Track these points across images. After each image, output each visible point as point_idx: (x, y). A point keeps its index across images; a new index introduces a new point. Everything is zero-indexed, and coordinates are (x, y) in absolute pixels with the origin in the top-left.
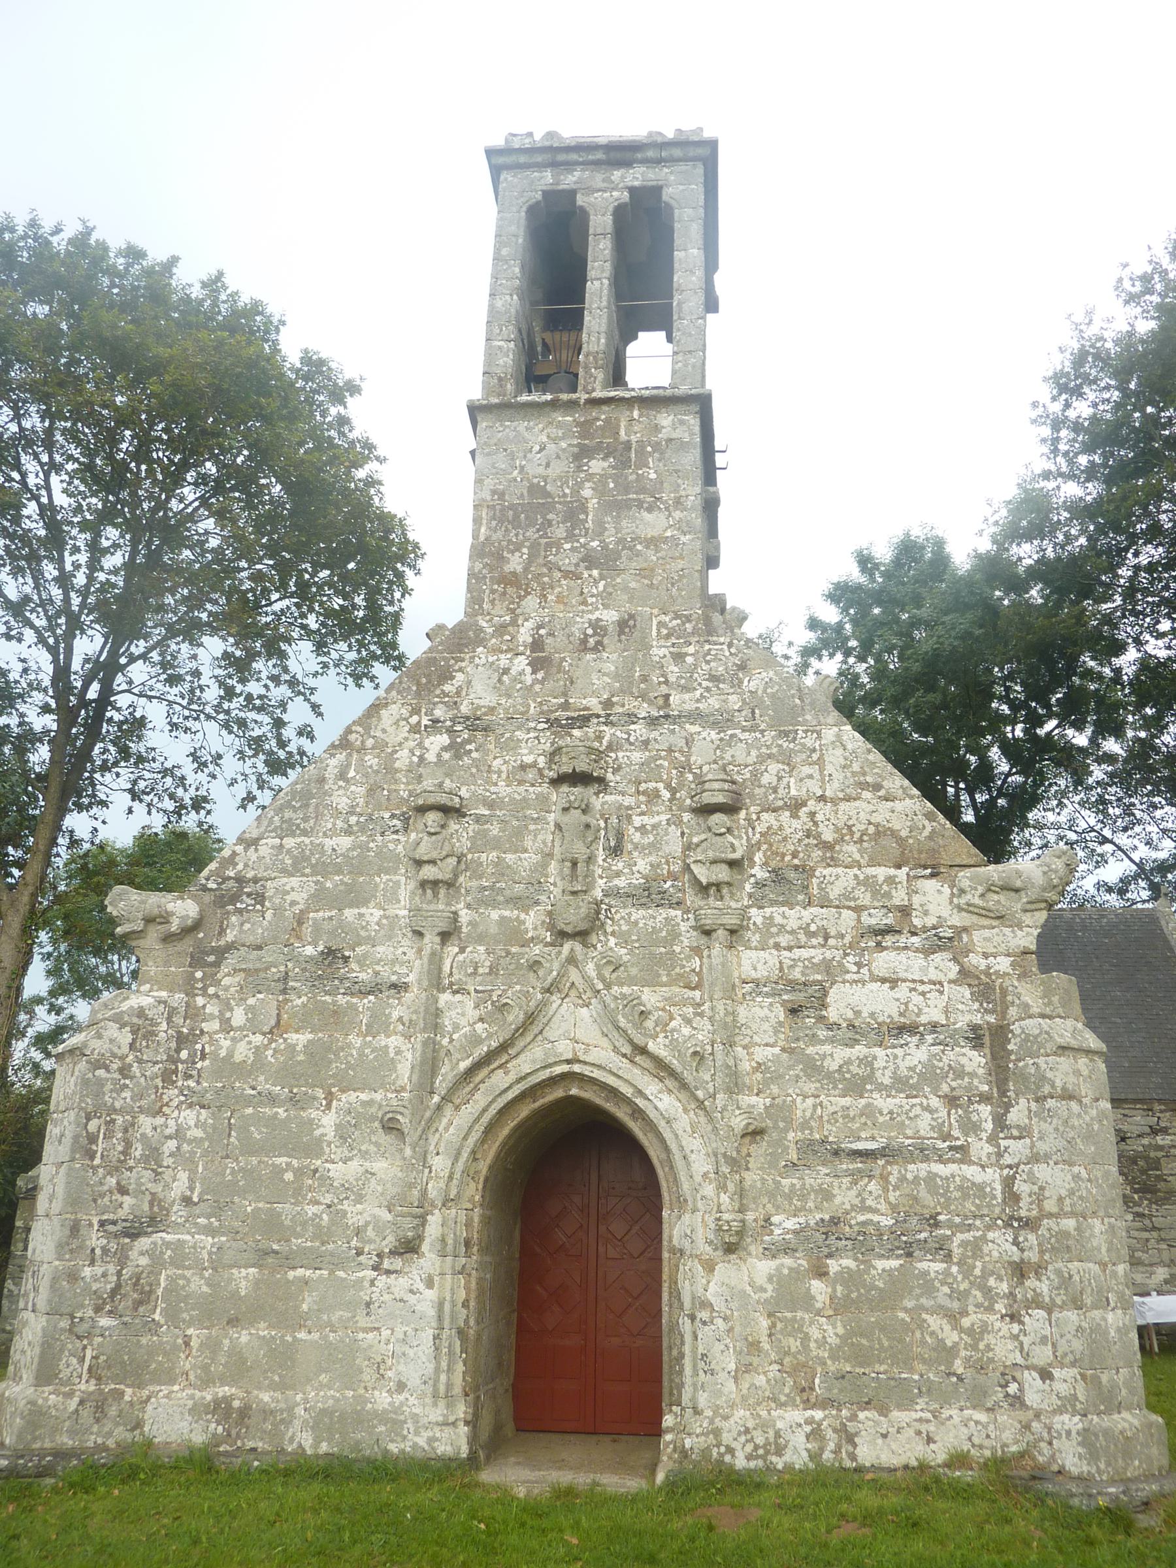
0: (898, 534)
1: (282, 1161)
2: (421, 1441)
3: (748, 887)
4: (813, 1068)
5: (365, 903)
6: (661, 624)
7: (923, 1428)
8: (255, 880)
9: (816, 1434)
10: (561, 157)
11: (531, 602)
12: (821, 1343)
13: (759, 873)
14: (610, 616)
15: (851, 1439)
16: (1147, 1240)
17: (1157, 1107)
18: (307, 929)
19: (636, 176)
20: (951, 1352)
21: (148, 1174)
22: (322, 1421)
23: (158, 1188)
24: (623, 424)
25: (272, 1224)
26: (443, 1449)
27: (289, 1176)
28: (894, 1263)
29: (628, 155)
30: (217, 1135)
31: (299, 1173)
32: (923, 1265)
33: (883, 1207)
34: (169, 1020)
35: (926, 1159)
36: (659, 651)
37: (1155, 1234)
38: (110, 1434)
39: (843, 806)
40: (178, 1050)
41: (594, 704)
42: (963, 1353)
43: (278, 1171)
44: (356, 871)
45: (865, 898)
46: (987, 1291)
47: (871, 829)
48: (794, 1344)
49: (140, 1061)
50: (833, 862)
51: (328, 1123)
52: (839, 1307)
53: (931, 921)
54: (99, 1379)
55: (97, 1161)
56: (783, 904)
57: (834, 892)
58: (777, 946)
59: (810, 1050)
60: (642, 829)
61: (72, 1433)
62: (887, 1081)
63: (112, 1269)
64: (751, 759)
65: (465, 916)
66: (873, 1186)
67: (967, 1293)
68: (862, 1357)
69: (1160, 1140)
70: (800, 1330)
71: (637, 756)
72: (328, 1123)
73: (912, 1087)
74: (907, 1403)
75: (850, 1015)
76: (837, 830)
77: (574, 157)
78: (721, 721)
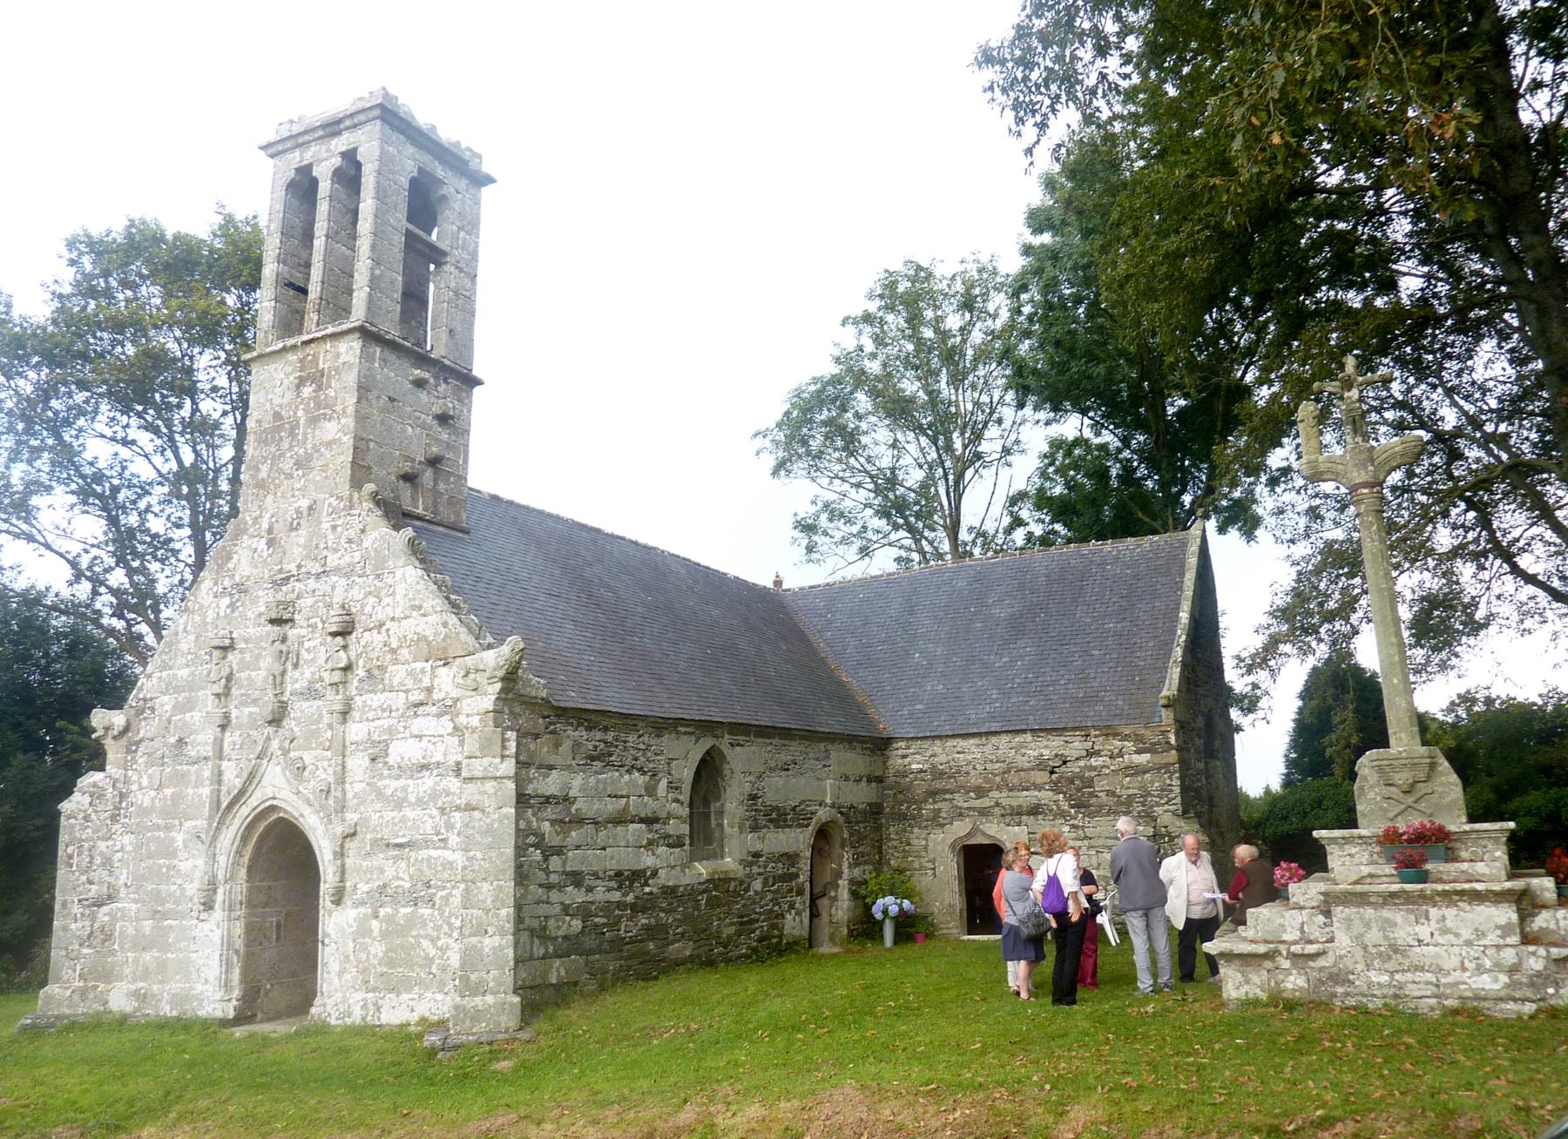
1: (161, 861)
2: (210, 1010)
3: (355, 683)
4: (380, 794)
5: (191, 710)
6: (330, 505)
7: (411, 1003)
8: (151, 699)
9: (364, 1007)
10: (301, 140)
11: (270, 498)
12: (376, 955)
14: (304, 503)
15: (378, 1009)
17: (1093, 733)
18: (172, 727)
19: (341, 144)
20: (431, 961)
21: (106, 872)
22: (177, 1000)
23: (112, 880)
24: (322, 355)
25: (158, 897)
27: (164, 870)
28: (409, 910)
29: (329, 130)
30: (138, 847)
31: (168, 868)
32: (422, 911)
33: (406, 877)
34: (114, 786)
35: (427, 848)
36: (326, 526)
37: (1086, 842)
38: (90, 1007)
39: (404, 622)
40: (120, 802)
41: (292, 567)
42: (437, 961)
43: (161, 867)
44: (191, 690)
45: (410, 684)
46: (450, 925)
47: (416, 637)
48: (363, 956)
49: (96, 812)
50: (395, 662)
51: (180, 838)
52: (385, 935)
53: (442, 695)
54: (85, 980)
55: (74, 868)
56: (371, 692)
57: (396, 682)
58: (367, 720)
59: (379, 783)
60: (308, 650)
61: (69, 1007)
62: (413, 800)
63: (87, 923)
64: (362, 596)
66: (403, 865)
67: (441, 926)
68: (391, 964)
69: (1094, 762)
70: (366, 949)
72: (180, 838)
73: (425, 803)
74: (409, 990)
75: (399, 760)
76: (399, 640)
77: (307, 138)
78: (348, 572)
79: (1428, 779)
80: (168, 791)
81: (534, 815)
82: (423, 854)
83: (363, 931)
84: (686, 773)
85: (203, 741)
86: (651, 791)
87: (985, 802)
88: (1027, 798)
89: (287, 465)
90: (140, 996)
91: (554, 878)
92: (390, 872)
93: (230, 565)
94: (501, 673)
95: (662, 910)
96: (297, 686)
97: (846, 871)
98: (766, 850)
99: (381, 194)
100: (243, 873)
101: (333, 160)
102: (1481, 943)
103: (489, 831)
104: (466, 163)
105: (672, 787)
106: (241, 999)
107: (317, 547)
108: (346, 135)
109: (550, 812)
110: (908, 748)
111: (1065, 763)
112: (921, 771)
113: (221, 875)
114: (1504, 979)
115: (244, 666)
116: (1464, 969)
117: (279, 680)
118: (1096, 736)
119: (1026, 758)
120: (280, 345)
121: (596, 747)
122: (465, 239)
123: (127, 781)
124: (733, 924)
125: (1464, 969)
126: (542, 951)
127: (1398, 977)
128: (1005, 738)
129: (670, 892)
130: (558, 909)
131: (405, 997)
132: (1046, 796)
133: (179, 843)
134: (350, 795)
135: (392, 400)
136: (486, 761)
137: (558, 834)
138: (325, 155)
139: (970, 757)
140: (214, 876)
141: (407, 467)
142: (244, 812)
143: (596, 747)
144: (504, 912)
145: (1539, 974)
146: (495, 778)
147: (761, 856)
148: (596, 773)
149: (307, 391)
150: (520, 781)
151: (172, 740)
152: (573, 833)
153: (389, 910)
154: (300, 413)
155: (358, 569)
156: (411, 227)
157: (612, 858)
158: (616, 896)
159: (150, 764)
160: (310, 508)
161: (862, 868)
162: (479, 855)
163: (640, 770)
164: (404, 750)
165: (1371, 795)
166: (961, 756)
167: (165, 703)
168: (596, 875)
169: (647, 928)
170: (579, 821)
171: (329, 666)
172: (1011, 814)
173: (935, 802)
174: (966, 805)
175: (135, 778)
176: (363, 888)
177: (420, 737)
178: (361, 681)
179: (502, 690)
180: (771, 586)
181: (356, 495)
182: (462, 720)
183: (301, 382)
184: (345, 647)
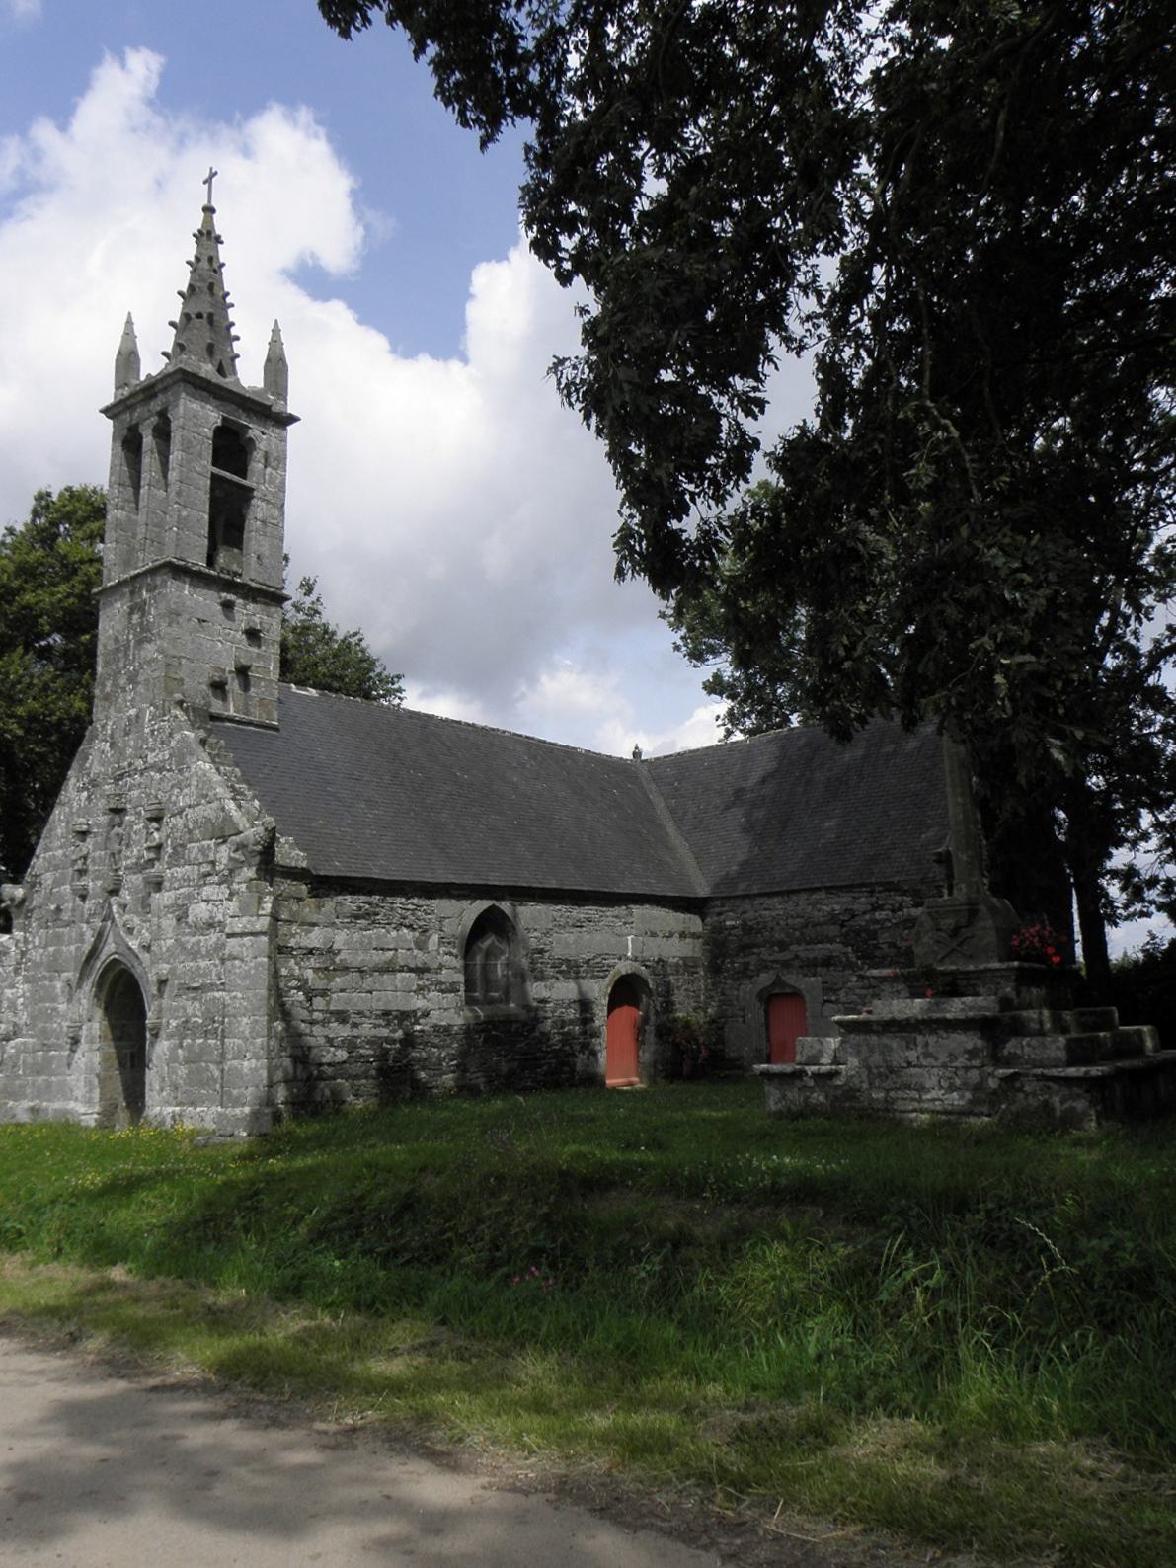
13: (169, 850)
16: (866, 996)
17: (878, 888)
28: (201, 1040)
33: (200, 1014)
34: (16, 946)
37: (870, 991)
39: (196, 809)
77: (133, 401)
79: (969, 924)
81: (296, 964)
83: (172, 1059)
86: (421, 945)
87: (787, 955)
88: (820, 950)
89: (122, 682)
91: (317, 1015)
93: (87, 765)
97: (653, 1018)
98: (554, 997)
102: (954, 1065)
103: (246, 976)
104: (269, 407)
107: (142, 748)
109: (313, 961)
110: (722, 906)
111: (853, 917)
112: (733, 927)
114: (968, 1095)
118: (880, 892)
119: (821, 914)
121: (360, 908)
124: (515, 1060)
127: (892, 1094)
128: (804, 896)
132: (836, 948)
136: (245, 920)
137: (322, 979)
138: (147, 414)
139: (774, 914)
142: (98, 965)
143: (360, 908)
144: (259, 1040)
145: (995, 1092)
146: (252, 934)
147: (548, 1003)
148: (361, 929)
149: (136, 618)
150: (272, 932)
151: (53, 907)
153: (189, 1041)
154: (131, 637)
156: (216, 470)
157: (379, 1000)
158: (385, 1032)
159: (40, 927)
160: (137, 716)
162: (239, 995)
163: (410, 927)
164: (200, 911)
165: (926, 939)
166: (767, 913)
167: (48, 878)
168: (360, 1013)
170: (345, 969)
172: (808, 966)
173: (745, 956)
174: (772, 958)
176: (173, 1023)
178: (170, 857)
179: (260, 863)
180: (629, 757)
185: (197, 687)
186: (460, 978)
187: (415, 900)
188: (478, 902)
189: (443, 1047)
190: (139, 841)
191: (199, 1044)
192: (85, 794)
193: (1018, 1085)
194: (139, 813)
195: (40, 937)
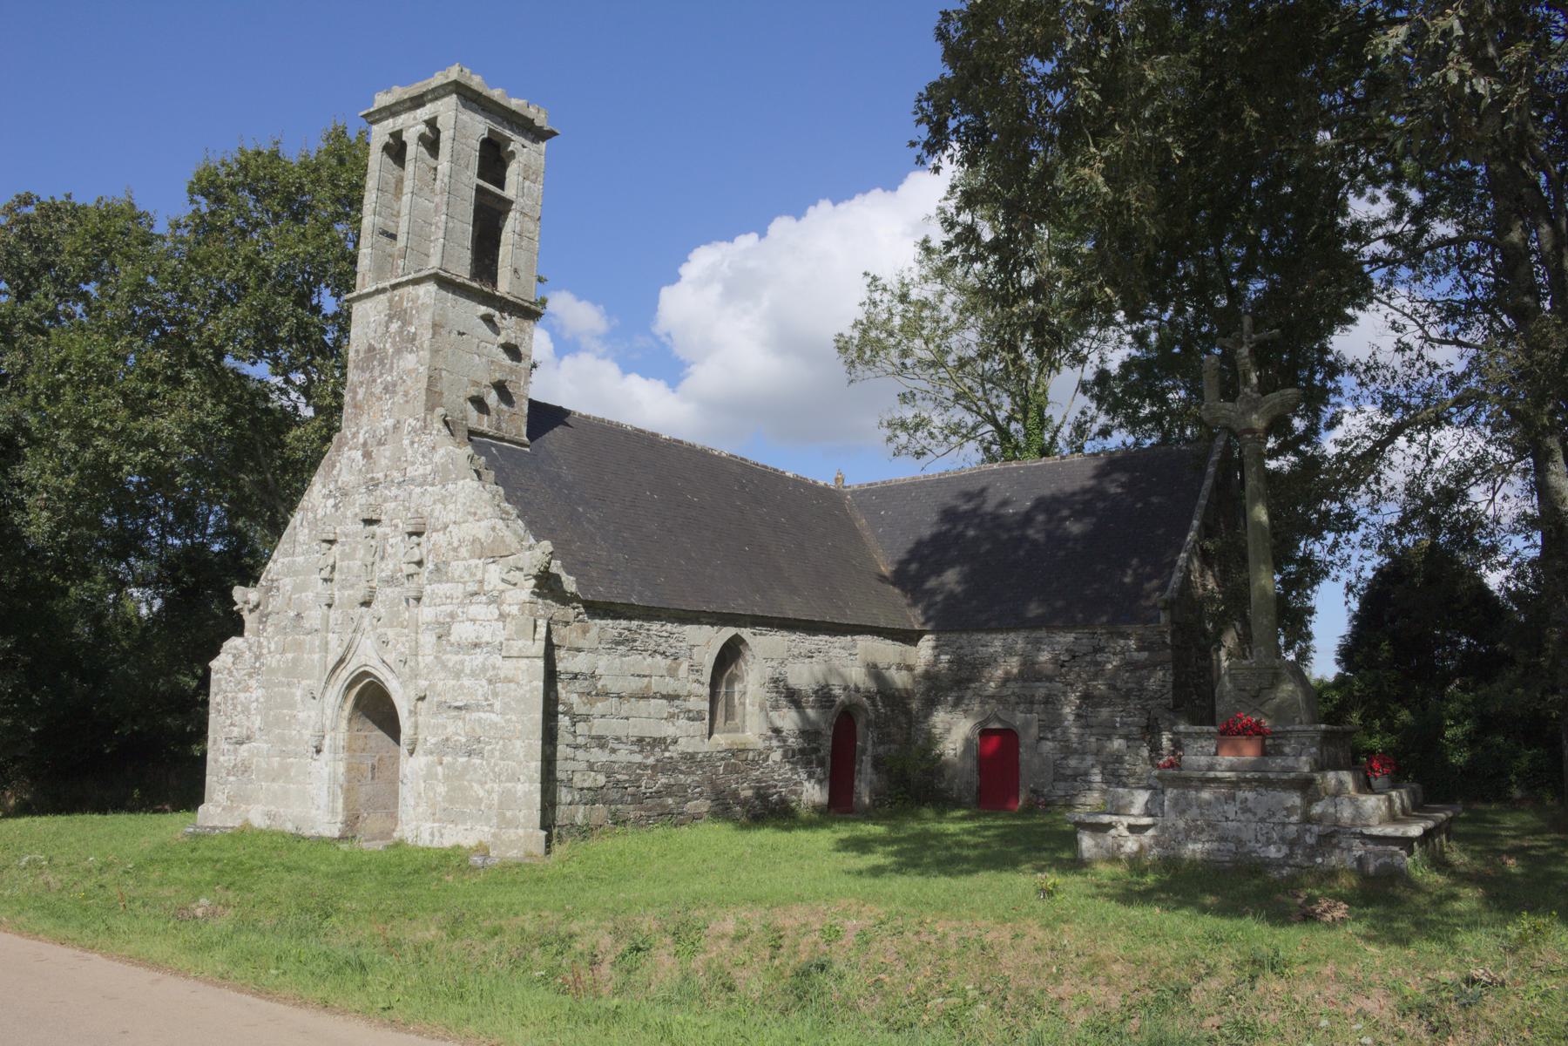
0: (804, 221)
4: (444, 666)
5: (305, 591)
9: (432, 834)
14: (390, 422)
15: (442, 836)
19: (425, 112)
20: (481, 800)
25: (283, 740)
26: (327, 834)
50: (457, 558)
51: (298, 693)
52: (447, 778)
53: (491, 587)
60: (392, 546)
62: (468, 672)
65: (337, 595)
66: (460, 723)
71: (393, 505)
72: (298, 693)
74: (464, 822)
80: (290, 656)
82: (475, 715)
83: (430, 776)
84: (708, 660)
85: (314, 617)
86: (672, 672)
89: (378, 389)
90: (268, 815)
91: (580, 740)
92: (450, 730)
93: (335, 472)
94: (535, 571)
95: (682, 772)
96: (383, 575)
97: (870, 748)
99: (454, 159)
100: (344, 724)
101: (418, 127)
105: (693, 669)
106: (345, 823)
107: (399, 459)
108: (429, 106)
109: (579, 685)
113: (328, 723)
115: (344, 556)
116: (1257, 841)
117: (369, 567)
120: (374, 288)
121: (620, 634)
122: (529, 187)
123: (260, 646)
125: (1257, 841)
126: (569, 798)
129: (690, 758)
130: (584, 765)
131: (461, 827)
133: (298, 698)
134: (422, 665)
135: (461, 334)
136: (520, 643)
137: (585, 704)
138: (413, 122)
140: (323, 725)
141: (473, 391)
142: (345, 675)
143: (620, 634)
149: (394, 326)
151: (292, 614)
152: (599, 704)
155: (430, 479)
156: (481, 182)
157: (635, 726)
158: (638, 758)
161: (887, 747)
162: (514, 718)
164: (462, 631)
167: (287, 583)
168: (618, 739)
169: (668, 786)
171: (405, 560)
175: (265, 643)
177: (474, 621)
181: (429, 417)
182: (506, 608)
183: (391, 318)
184: (418, 545)
185: (456, 400)
186: (706, 706)
187: (669, 627)
188: (725, 629)
189: (689, 774)
190: (395, 554)
191: (462, 763)
192: (331, 502)
193: (1335, 841)
194: (396, 526)
195: (276, 643)
